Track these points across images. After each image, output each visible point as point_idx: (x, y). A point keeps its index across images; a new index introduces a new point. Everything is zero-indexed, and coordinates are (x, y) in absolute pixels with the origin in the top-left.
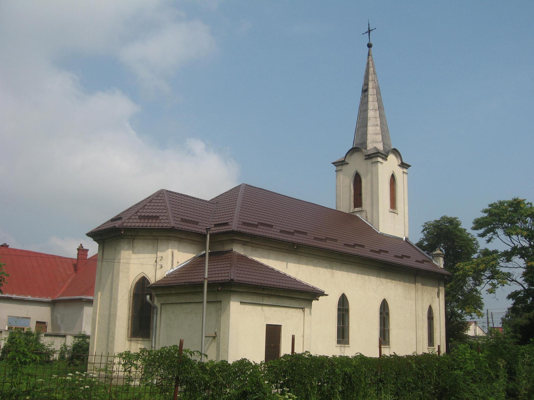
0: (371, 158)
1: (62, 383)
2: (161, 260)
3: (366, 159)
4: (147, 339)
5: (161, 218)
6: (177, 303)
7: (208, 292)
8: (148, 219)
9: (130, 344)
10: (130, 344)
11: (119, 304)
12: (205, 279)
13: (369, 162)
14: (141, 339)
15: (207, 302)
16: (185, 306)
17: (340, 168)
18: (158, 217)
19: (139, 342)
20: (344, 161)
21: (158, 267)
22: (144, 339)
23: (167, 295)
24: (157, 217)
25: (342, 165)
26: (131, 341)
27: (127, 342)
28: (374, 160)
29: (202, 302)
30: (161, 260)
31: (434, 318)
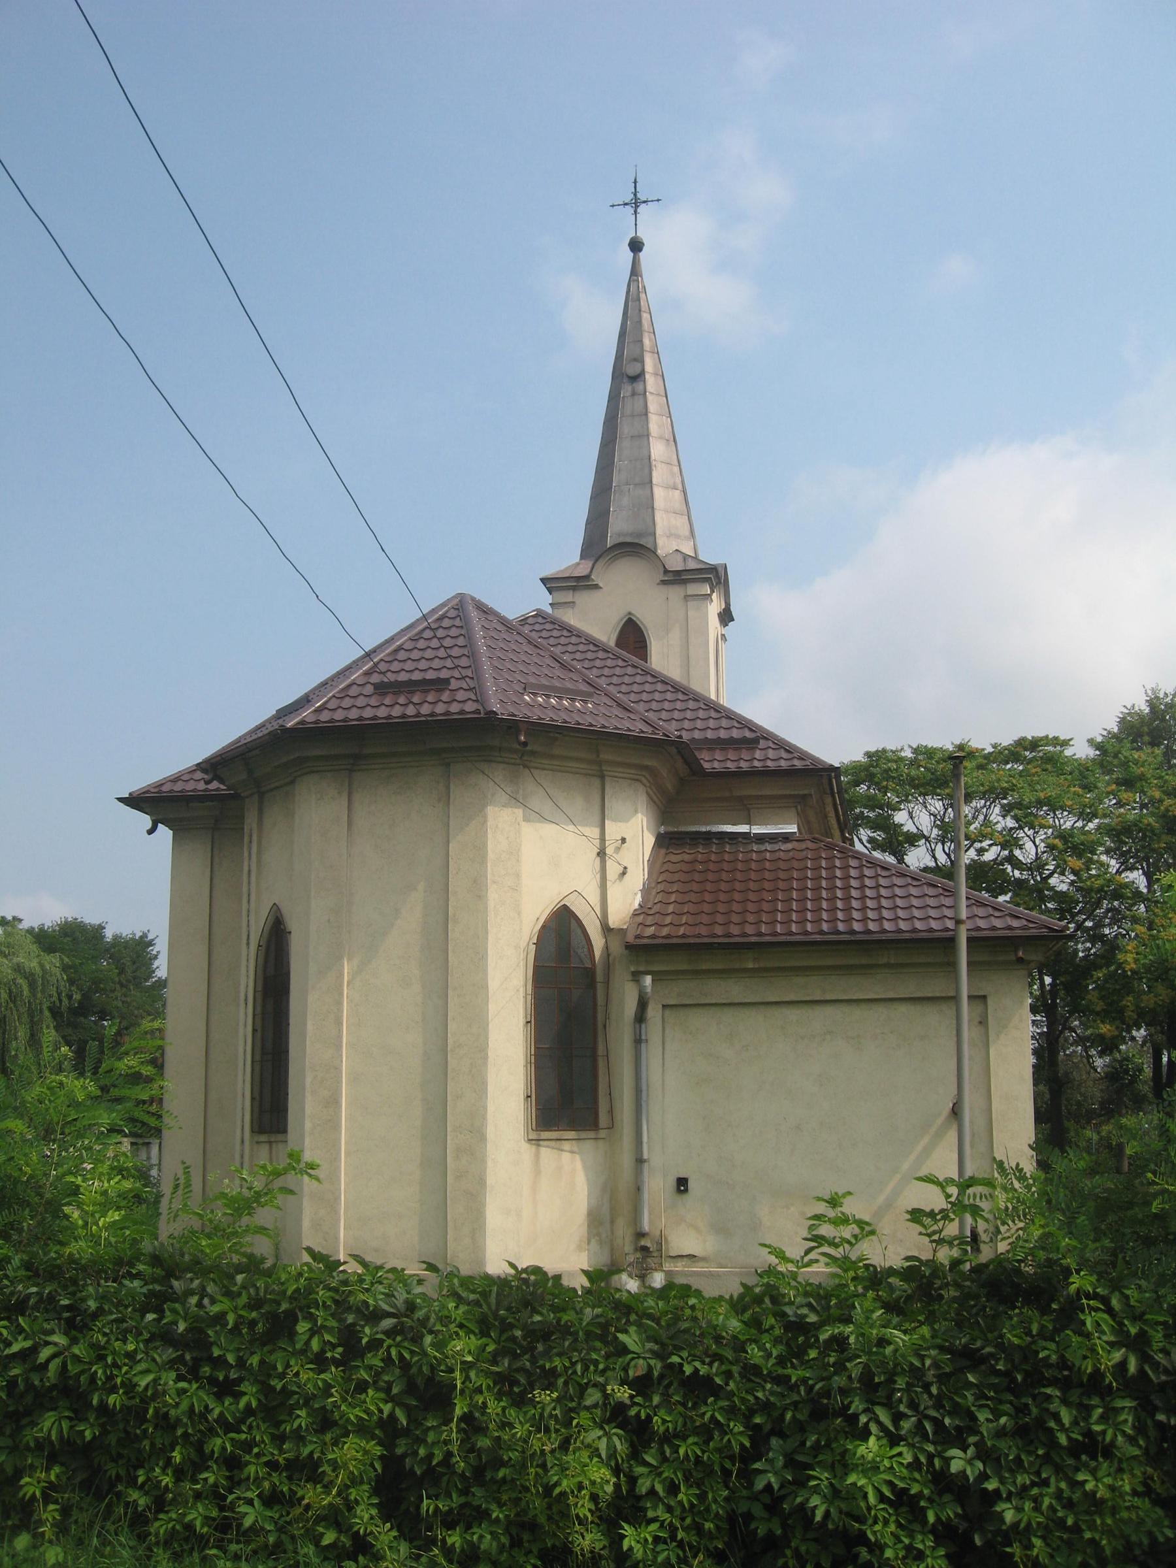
0: (684, 582)
1: (358, 1311)
2: (618, 849)
3: (664, 582)
4: (591, 1134)
5: (454, 684)
6: (777, 1003)
7: (970, 964)
8: (426, 692)
9: (537, 1156)
10: (537, 1156)
11: (492, 1008)
12: (958, 922)
13: (675, 593)
14: (571, 1134)
15: (969, 997)
16: (793, 1014)
17: (567, 596)
18: (447, 681)
19: (567, 1146)
20: (587, 577)
21: (613, 870)
22: (583, 1135)
23: (696, 973)
24: (440, 684)
25: (574, 588)
26: (536, 1142)
27: (525, 1146)
28: (692, 589)
29: (955, 999)
30: (618, 849)
31: (522, 1098)
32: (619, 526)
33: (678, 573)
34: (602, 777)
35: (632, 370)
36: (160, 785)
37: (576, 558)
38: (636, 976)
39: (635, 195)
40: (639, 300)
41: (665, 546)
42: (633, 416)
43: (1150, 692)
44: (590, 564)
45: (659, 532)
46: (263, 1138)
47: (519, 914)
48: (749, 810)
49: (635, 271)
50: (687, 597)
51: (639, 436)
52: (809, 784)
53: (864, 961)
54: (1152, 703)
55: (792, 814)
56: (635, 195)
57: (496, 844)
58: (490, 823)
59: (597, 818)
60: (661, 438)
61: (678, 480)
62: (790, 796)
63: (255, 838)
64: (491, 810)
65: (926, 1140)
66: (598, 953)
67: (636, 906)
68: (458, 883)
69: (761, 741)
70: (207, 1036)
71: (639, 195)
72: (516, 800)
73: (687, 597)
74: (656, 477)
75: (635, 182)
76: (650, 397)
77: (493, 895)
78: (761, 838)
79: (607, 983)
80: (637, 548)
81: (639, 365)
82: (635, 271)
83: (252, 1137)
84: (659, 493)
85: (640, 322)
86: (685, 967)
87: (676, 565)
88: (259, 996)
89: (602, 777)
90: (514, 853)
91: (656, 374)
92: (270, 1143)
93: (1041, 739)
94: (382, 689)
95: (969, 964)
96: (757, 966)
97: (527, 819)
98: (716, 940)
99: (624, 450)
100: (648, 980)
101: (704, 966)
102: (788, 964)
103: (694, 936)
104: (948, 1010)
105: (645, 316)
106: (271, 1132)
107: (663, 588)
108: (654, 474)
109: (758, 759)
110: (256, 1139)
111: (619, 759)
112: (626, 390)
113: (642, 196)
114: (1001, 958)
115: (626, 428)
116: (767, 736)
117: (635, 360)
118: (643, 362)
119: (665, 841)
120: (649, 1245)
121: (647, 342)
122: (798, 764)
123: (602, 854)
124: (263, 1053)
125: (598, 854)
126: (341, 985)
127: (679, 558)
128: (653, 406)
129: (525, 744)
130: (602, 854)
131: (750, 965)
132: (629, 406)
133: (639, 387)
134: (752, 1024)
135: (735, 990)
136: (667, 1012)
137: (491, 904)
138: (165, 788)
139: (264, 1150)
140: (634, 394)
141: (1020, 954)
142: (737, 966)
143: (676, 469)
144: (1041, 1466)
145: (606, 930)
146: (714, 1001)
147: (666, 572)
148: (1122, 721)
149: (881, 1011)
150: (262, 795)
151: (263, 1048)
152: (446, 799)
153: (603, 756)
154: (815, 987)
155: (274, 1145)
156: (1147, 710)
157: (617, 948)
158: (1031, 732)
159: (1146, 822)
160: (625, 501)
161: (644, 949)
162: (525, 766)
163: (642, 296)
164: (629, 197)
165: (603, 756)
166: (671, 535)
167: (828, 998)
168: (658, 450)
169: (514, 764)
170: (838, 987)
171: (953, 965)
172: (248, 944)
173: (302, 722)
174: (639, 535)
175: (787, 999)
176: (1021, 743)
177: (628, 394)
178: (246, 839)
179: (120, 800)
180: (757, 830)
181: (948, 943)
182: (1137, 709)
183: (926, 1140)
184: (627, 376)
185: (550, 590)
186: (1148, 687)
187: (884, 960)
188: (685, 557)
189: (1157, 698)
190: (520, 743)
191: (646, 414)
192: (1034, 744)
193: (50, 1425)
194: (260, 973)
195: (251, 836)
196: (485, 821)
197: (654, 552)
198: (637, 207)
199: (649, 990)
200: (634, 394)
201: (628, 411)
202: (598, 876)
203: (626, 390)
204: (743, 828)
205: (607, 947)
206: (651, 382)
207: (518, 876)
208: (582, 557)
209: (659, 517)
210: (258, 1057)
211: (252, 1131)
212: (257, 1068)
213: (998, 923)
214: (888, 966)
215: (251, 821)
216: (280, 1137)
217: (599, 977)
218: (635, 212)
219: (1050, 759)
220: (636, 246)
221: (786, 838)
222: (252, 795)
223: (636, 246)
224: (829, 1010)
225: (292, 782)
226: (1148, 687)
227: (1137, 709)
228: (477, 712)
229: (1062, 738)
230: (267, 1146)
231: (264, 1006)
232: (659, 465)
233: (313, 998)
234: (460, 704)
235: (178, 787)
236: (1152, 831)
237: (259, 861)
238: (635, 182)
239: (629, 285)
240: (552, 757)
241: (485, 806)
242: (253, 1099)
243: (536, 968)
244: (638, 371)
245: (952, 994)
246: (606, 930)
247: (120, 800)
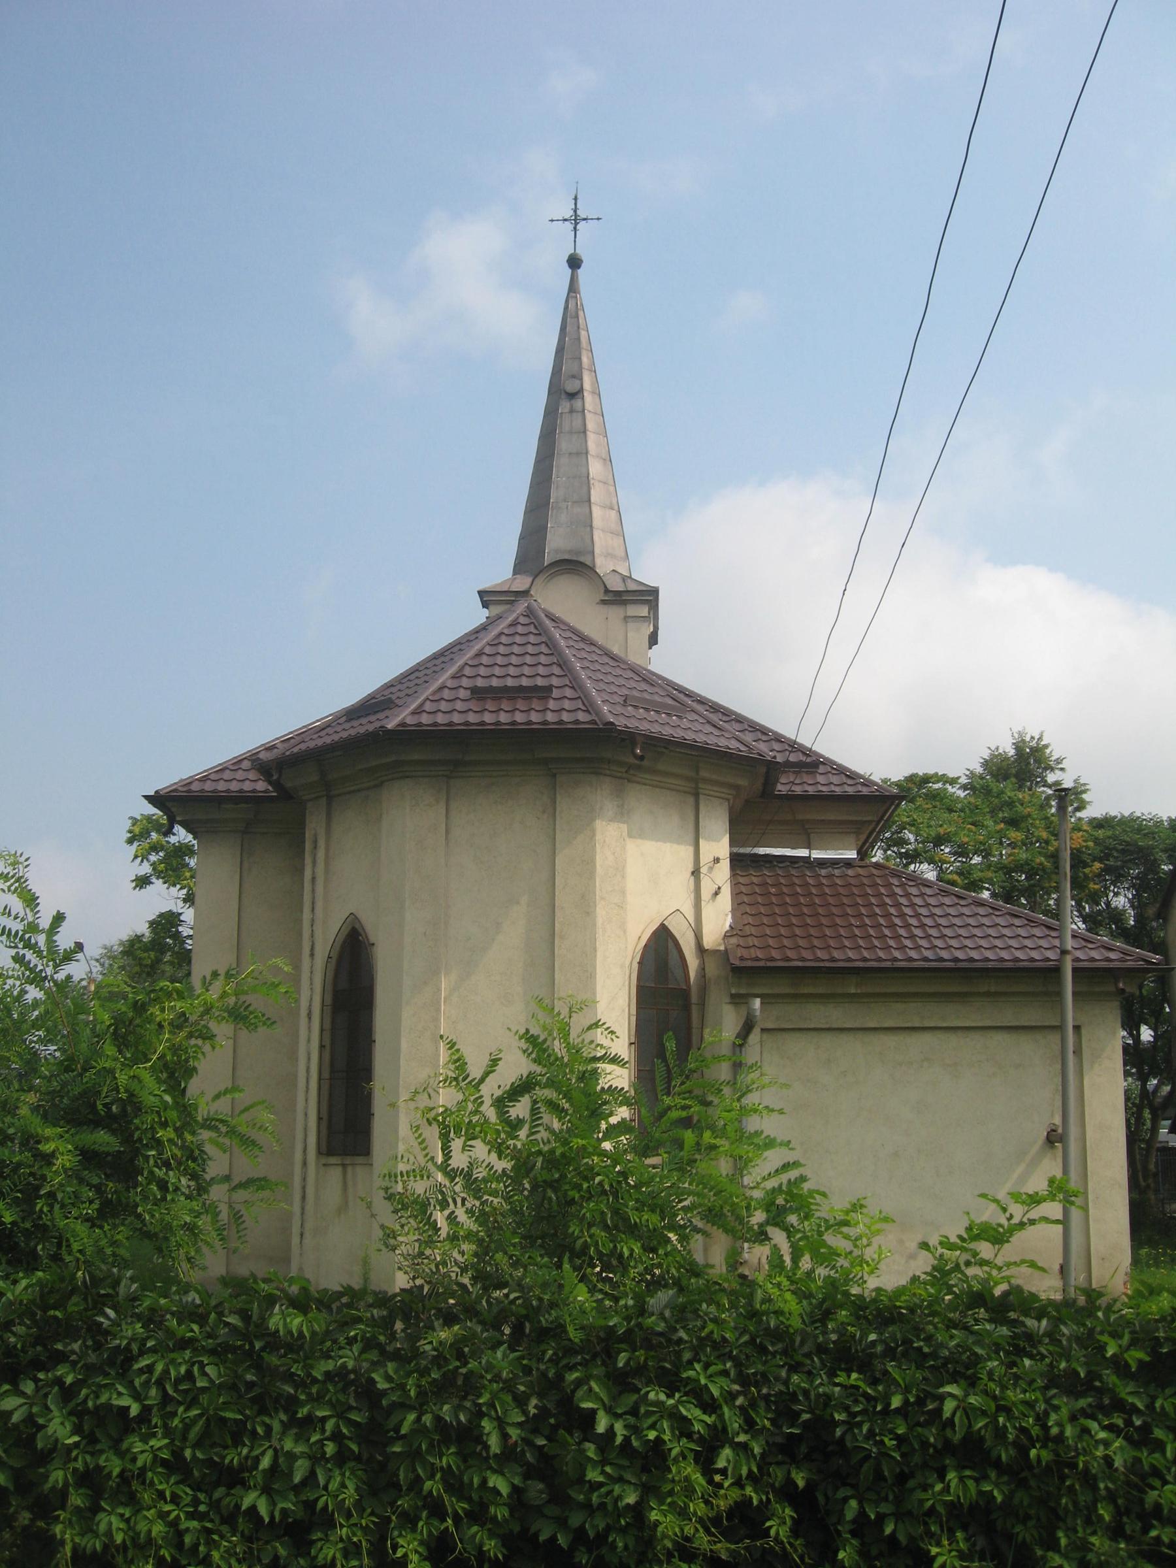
0: (624, 603)
2: (711, 869)
3: (604, 602)
6: (908, 1028)
12: (1064, 952)
13: (615, 613)
16: (891, 1040)
18: (550, 688)
23: (795, 997)
24: (544, 693)
28: (632, 610)
29: (1060, 1028)
30: (711, 869)
32: (557, 543)
33: (618, 593)
34: (696, 795)
35: (571, 386)
36: (189, 783)
37: (508, 573)
38: (738, 1000)
39: (575, 211)
40: (577, 317)
41: (603, 566)
42: (571, 432)
43: (1016, 736)
44: (530, 579)
45: (597, 551)
46: (333, 1160)
47: (625, 932)
48: (808, 835)
49: (573, 288)
50: (626, 619)
51: (578, 454)
52: (870, 808)
53: (965, 989)
54: (1019, 747)
55: (851, 839)
56: (575, 211)
57: (603, 859)
58: (598, 837)
59: (690, 836)
60: (598, 456)
61: (614, 502)
62: (851, 822)
63: (322, 843)
64: (599, 824)
65: (1020, 1169)
66: (692, 975)
67: (727, 928)
68: (563, 899)
69: (821, 766)
70: (235, 1051)
71: (578, 212)
72: (622, 814)
73: (626, 619)
74: (595, 496)
75: (576, 199)
76: (588, 416)
77: (601, 912)
78: (822, 863)
79: (702, 1004)
80: (576, 566)
81: (578, 382)
82: (573, 288)
83: (317, 1158)
84: (597, 512)
85: (579, 339)
86: (788, 990)
87: (616, 585)
88: (328, 1010)
89: (696, 795)
90: (620, 869)
91: (593, 393)
92: (344, 1166)
93: (932, 776)
94: (478, 694)
95: (1074, 993)
96: (793, 992)
97: (630, 836)
98: (822, 964)
99: (562, 466)
100: (757, 1003)
101: (806, 991)
102: (888, 991)
103: (751, 959)
104: (1055, 1038)
105: (583, 333)
106: (345, 1153)
107: (604, 609)
108: (592, 492)
109: (822, 783)
110: (324, 1160)
111: (714, 777)
112: (564, 406)
113: (582, 213)
114: (1097, 989)
115: (564, 444)
116: (828, 762)
117: (574, 377)
118: (581, 379)
119: (738, 862)
120: (747, 1273)
121: (585, 360)
122: (865, 791)
123: (696, 873)
124: (332, 1071)
125: (693, 873)
126: (439, 1003)
127: (618, 579)
128: (591, 425)
129: (642, 758)
130: (696, 873)
131: (853, 991)
132: (566, 423)
133: (577, 404)
134: (850, 1050)
135: (834, 1015)
136: (765, 1036)
137: (599, 922)
138: (195, 787)
139: (335, 1174)
140: (572, 411)
141: (1121, 985)
142: (839, 991)
143: (612, 489)
144: (12, 1468)
145: (701, 950)
146: (812, 1026)
147: (607, 591)
148: (986, 764)
149: (976, 1040)
150: (330, 799)
151: (332, 1064)
152: (551, 811)
153: (704, 774)
154: (912, 1013)
155: (349, 1169)
156: (1012, 752)
157: (712, 970)
158: (922, 769)
159: (1038, 861)
160: (563, 517)
161: (744, 972)
162: (629, 781)
163: (581, 313)
164: (569, 213)
165: (704, 774)
166: (609, 555)
167: (927, 1025)
168: (595, 468)
169: (620, 778)
170: (934, 1014)
171: (1059, 994)
172: (312, 955)
173: (403, 724)
174: (578, 553)
175: (886, 1025)
176: (911, 779)
177: (567, 410)
178: (308, 846)
179: (146, 797)
180: (816, 854)
181: (1052, 973)
182: (1048, 751)
183: (1020, 1169)
184: (565, 391)
185: (485, 605)
186: (1015, 730)
187: (983, 988)
188: (624, 579)
189: (1023, 741)
190: (636, 756)
191: (585, 432)
192: (926, 779)
193: (956, 1485)
194: (329, 988)
195: (315, 842)
196: (594, 835)
197: (592, 569)
198: (576, 224)
199: (758, 1013)
200: (572, 411)
201: (566, 427)
202: (692, 896)
203: (564, 406)
204: (803, 853)
205: (702, 969)
206: (588, 398)
207: (623, 892)
208: (515, 572)
209: (598, 536)
210: (326, 1075)
211: (319, 1152)
212: (326, 1087)
213: (1095, 954)
214: (988, 994)
215: (314, 824)
216: (360, 1160)
217: (694, 998)
218: (575, 228)
219: (934, 796)
220: (574, 262)
221: (848, 863)
222: (317, 798)
223: (574, 262)
224: (927, 1037)
225: (381, 785)
226: (1015, 730)
227: (1001, 751)
228: (593, 722)
229: (951, 776)
230: (339, 1169)
231: (333, 1022)
232: (596, 484)
233: (407, 1016)
234: (560, 712)
235: (208, 786)
236: (1044, 870)
237: (327, 871)
238: (576, 199)
239: (567, 301)
240: (655, 772)
241: (593, 820)
242: (320, 1119)
243: (640, 988)
244: (577, 388)
245: (1055, 1022)
246: (701, 950)
247: (146, 797)
